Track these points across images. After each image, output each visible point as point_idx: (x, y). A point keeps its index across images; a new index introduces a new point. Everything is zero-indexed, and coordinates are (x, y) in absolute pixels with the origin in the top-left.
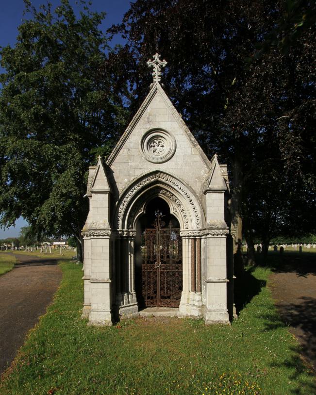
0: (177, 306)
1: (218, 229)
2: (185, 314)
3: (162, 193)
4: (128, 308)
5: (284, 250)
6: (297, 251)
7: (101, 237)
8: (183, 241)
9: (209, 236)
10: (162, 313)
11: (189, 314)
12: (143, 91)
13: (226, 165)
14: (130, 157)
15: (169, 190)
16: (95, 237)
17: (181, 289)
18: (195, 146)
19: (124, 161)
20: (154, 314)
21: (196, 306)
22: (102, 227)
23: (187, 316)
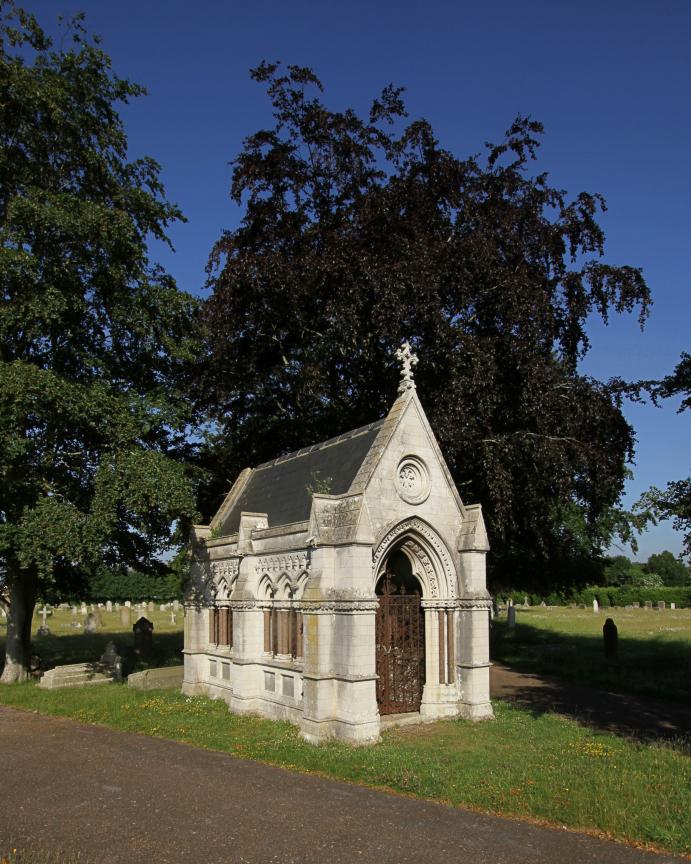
0: (416, 707)
1: (483, 599)
2: (435, 717)
3: (408, 546)
4: (312, 723)
5: (156, 631)
6: (129, 634)
7: (366, 612)
8: (427, 614)
9: (474, 608)
10: (408, 719)
11: (442, 716)
12: (375, 403)
13: (266, 515)
14: (382, 491)
15: (423, 545)
16: (360, 612)
17: (423, 680)
18: (450, 486)
19: (376, 496)
20: (398, 722)
21: (452, 702)
22: (369, 597)
23: (439, 719)
